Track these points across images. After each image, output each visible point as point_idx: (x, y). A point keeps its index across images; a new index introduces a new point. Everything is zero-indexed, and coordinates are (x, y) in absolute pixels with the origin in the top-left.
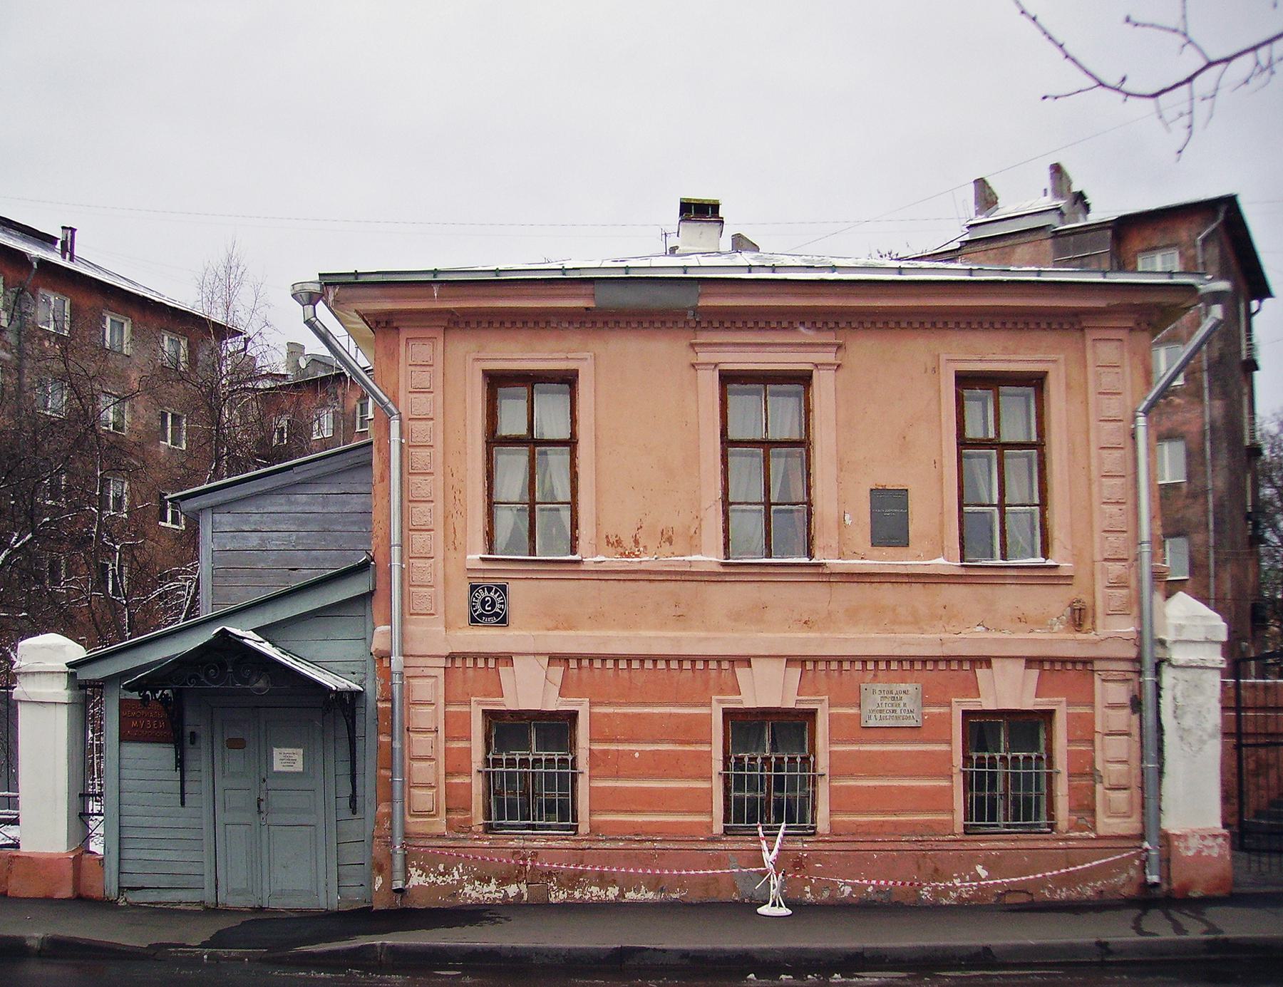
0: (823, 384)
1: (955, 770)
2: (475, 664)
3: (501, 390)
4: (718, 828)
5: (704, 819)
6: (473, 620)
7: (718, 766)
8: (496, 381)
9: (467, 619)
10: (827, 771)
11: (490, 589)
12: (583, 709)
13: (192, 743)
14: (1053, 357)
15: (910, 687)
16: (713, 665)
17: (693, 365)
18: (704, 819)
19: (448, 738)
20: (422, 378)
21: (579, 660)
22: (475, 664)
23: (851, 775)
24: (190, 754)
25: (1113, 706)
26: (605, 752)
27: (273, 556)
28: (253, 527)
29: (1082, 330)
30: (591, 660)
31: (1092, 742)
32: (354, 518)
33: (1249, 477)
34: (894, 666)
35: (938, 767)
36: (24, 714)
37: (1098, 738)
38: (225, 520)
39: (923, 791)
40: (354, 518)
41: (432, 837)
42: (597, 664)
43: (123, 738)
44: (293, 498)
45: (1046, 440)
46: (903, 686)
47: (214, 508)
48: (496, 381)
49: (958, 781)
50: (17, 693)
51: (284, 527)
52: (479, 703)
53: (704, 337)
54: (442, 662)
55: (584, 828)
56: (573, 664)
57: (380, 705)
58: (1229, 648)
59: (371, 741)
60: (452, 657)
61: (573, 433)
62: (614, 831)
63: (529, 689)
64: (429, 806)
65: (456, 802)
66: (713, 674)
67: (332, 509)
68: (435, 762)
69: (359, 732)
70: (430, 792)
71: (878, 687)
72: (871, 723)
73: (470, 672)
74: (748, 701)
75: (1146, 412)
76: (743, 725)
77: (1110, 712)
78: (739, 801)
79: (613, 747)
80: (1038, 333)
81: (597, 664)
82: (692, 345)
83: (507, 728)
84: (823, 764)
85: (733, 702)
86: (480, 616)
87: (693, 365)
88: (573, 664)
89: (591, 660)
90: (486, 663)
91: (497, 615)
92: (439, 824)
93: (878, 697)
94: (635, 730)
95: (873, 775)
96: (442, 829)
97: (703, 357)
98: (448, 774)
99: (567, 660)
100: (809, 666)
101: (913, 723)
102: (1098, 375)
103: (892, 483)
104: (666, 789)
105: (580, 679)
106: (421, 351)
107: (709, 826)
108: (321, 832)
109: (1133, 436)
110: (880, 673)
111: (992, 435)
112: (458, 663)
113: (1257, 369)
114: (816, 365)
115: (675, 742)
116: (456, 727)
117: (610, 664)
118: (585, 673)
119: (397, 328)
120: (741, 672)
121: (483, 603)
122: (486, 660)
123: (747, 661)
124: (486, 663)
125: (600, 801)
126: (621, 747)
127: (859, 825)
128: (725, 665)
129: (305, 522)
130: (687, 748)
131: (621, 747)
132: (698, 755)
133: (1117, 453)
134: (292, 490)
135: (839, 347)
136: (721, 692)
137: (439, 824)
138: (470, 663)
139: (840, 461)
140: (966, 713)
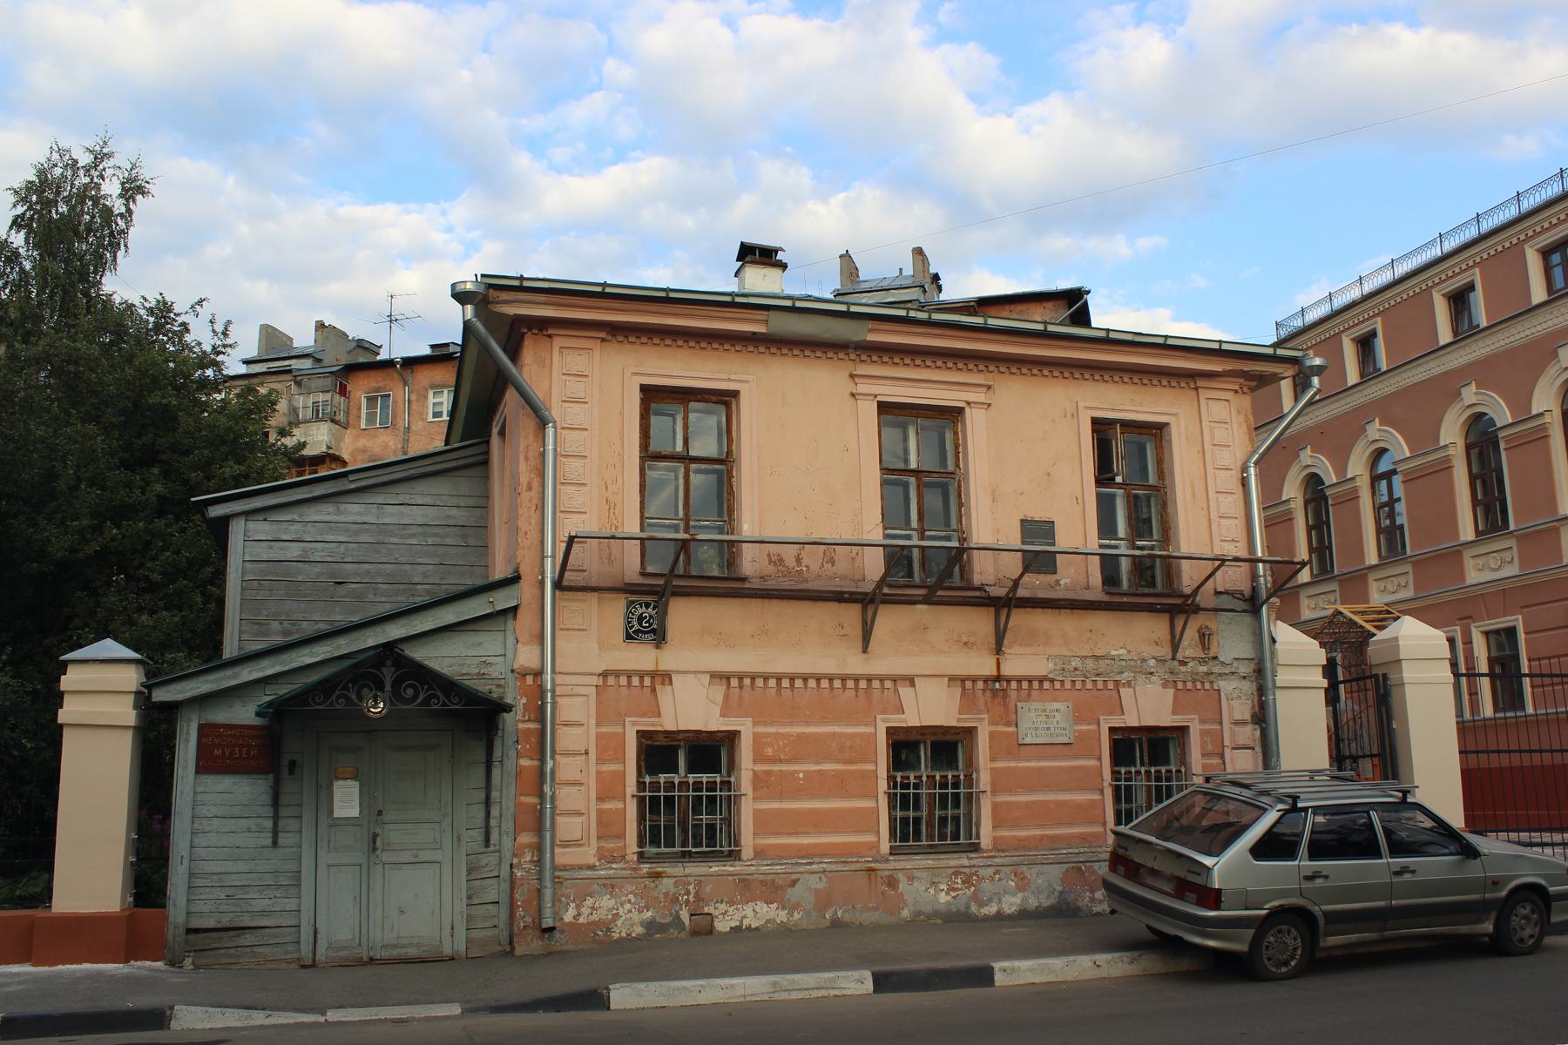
0: (974, 418)
1: (1106, 784)
2: (629, 682)
3: (653, 406)
4: (885, 847)
5: (871, 838)
6: (629, 637)
7: (883, 785)
8: (652, 396)
9: (621, 635)
10: (988, 788)
11: (647, 605)
12: (746, 729)
13: (291, 772)
14: (1173, 411)
15: (1061, 706)
16: (876, 684)
17: (853, 395)
18: (871, 838)
19: (600, 760)
20: (576, 388)
21: (741, 678)
22: (629, 682)
23: (1010, 791)
24: (289, 786)
25: (1237, 723)
26: (769, 773)
27: (317, 568)
28: (294, 537)
29: (1196, 389)
30: (753, 679)
31: (1222, 756)
32: (414, 530)
33: (957, 569)
34: (1046, 685)
35: (1085, 780)
36: (69, 741)
37: (1227, 752)
38: (260, 528)
39: (1079, 806)
40: (414, 530)
41: (581, 868)
42: (760, 682)
43: (200, 770)
44: (342, 507)
45: (1167, 482)
46: (1056, 705)
47: (248, 514)
48: (652, 396)
49: (1109, 793)
50: (63, 716)
51: (331, 538)
52: (634, 723)
53: (863, 369)
54: (595, 680)
55: (747, 853)
56: (734, 682)
57: (521, 726)
58: (1329, 670)
59: (510, 764)
60: (605, 675)
61: (729, 452)
62: (779, 854)
63: (691, 708)
64: (577, 835)
65: (608, 827)
66: (876, 693)
67: (387, 521)
68: (586, 786)
69: (497, 753)
70: (579, 819)
71: (1035, 705)
72: (1028, 741)
73: (624, 691)
74: (911, 719)
75: (1256, 463)
76: (904, 746)
77: (1237, 729)
78: (905, 821)
79: (776, 768)
80: (1158, 389)
81: (760, 682)
82: (852, 376)
83: (657, 752)
84: (984, 779)
85: (897, 721)
86: (637, 632)
87: (853, 395)
88: (734, 682)
89: (753, 679)
90: (642, 681)
91: (654, 631)
92: (588, 854)
93: (1033, 714)
94: (803, 748)
95: (1031, 789)
96: (593, 860)
97: (863, 387)
98: (600, 799)
99: (728, 679)
100: (969, 684)
101: (1066, 740)
102: (1212, 429)
103: (1038, 514)
104: (831, 810)
105: (740, 697)
106: (577, 362)
107: (876, 846)
108: (447, 869)
109: (1244, 483)
110: (1034, 693)
111: (679, 448)
112: (611, 680)
113: (1074, 302)
114: (969, 403)
115: (838, 761)
116: (608, 748)
117: (772, 683)
118: (747, 692)
119: (550, 336)
120: (905, 692)
121: (641, 618)
122: (642, 677)
123: (911, 680)
124: (642, 681)
125: (764, 823)
126: (784, 767)
127: (1020, 840)
128: (888, 684)
129: (356, 533)
130: (852, 767)
131: (784, 767)
132: (864, 775)
133: (1230, 498)
134: (339, 499)
135: (989, 387)
136: (884, 711)
137: (588, 854)
138: (623, 680)
139: (993, 493)
140: (1112, 729)
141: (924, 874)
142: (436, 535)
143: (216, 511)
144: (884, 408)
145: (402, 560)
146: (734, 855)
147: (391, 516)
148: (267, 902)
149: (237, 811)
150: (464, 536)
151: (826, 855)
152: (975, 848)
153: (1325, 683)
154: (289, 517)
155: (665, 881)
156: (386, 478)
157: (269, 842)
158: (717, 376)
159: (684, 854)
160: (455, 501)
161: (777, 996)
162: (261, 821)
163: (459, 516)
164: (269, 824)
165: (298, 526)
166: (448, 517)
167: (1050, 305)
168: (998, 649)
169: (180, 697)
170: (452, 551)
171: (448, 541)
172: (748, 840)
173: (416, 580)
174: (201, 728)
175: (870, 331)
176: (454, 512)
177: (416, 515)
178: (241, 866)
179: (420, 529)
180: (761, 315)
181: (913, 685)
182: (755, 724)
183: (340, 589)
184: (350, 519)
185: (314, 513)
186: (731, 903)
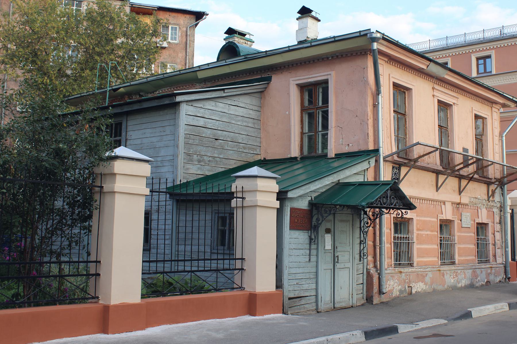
15: (468, 214)
27: (209, 132)
32: (240, 118)
44: (217, 103)
53: (437, 87)
82: (433, 88)
103: (466, 147)
114: (454, 104)
141: (448, 272)
142: (246, 122)
143: (179, 99)
144: (439, 101)
145: (236, 131)
146: (411, 265)
147: (233, 110)
148: (307, 285)
149: (300, 246)
150: (254, 123)
151: (429, 265)
152: (453, 263)
153: (147, 192)
154: (200, 106)
155: (403, 274)
156: (235, 93)
157: (308, 260)
158: (409, 82)
159: (400, 264)
160: (251, 107)
161: (497, 312)
162: (306, 250)
163: (253, 114)
164: (308, 252)
165: (202, 110)
166: (250, 114)
167: (188, 16)
168: (460, 192)
169: (295, 196)
170: (251, 129)
171: (250, 125)
172: (416, 259)
173: (240, 141)
174: (292, 209)
175: (447, 74)
176: (251, 112)
177: (240, 112)
178: (301, 270)
179: (241, 118)
180: (428, 63)
181: (444, 204)
182: (417, 216)
183: (216, 141)
184: (220, 110)
185: (209, 105)
186: (416, 283)
